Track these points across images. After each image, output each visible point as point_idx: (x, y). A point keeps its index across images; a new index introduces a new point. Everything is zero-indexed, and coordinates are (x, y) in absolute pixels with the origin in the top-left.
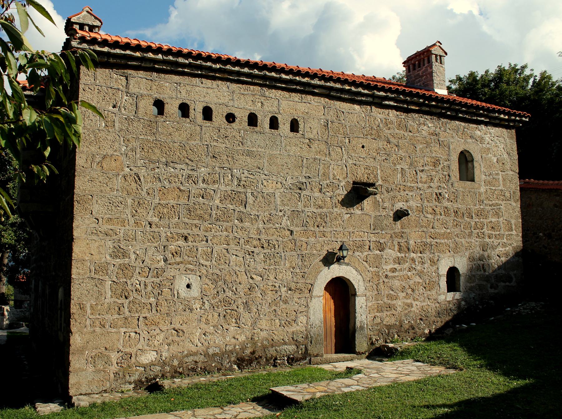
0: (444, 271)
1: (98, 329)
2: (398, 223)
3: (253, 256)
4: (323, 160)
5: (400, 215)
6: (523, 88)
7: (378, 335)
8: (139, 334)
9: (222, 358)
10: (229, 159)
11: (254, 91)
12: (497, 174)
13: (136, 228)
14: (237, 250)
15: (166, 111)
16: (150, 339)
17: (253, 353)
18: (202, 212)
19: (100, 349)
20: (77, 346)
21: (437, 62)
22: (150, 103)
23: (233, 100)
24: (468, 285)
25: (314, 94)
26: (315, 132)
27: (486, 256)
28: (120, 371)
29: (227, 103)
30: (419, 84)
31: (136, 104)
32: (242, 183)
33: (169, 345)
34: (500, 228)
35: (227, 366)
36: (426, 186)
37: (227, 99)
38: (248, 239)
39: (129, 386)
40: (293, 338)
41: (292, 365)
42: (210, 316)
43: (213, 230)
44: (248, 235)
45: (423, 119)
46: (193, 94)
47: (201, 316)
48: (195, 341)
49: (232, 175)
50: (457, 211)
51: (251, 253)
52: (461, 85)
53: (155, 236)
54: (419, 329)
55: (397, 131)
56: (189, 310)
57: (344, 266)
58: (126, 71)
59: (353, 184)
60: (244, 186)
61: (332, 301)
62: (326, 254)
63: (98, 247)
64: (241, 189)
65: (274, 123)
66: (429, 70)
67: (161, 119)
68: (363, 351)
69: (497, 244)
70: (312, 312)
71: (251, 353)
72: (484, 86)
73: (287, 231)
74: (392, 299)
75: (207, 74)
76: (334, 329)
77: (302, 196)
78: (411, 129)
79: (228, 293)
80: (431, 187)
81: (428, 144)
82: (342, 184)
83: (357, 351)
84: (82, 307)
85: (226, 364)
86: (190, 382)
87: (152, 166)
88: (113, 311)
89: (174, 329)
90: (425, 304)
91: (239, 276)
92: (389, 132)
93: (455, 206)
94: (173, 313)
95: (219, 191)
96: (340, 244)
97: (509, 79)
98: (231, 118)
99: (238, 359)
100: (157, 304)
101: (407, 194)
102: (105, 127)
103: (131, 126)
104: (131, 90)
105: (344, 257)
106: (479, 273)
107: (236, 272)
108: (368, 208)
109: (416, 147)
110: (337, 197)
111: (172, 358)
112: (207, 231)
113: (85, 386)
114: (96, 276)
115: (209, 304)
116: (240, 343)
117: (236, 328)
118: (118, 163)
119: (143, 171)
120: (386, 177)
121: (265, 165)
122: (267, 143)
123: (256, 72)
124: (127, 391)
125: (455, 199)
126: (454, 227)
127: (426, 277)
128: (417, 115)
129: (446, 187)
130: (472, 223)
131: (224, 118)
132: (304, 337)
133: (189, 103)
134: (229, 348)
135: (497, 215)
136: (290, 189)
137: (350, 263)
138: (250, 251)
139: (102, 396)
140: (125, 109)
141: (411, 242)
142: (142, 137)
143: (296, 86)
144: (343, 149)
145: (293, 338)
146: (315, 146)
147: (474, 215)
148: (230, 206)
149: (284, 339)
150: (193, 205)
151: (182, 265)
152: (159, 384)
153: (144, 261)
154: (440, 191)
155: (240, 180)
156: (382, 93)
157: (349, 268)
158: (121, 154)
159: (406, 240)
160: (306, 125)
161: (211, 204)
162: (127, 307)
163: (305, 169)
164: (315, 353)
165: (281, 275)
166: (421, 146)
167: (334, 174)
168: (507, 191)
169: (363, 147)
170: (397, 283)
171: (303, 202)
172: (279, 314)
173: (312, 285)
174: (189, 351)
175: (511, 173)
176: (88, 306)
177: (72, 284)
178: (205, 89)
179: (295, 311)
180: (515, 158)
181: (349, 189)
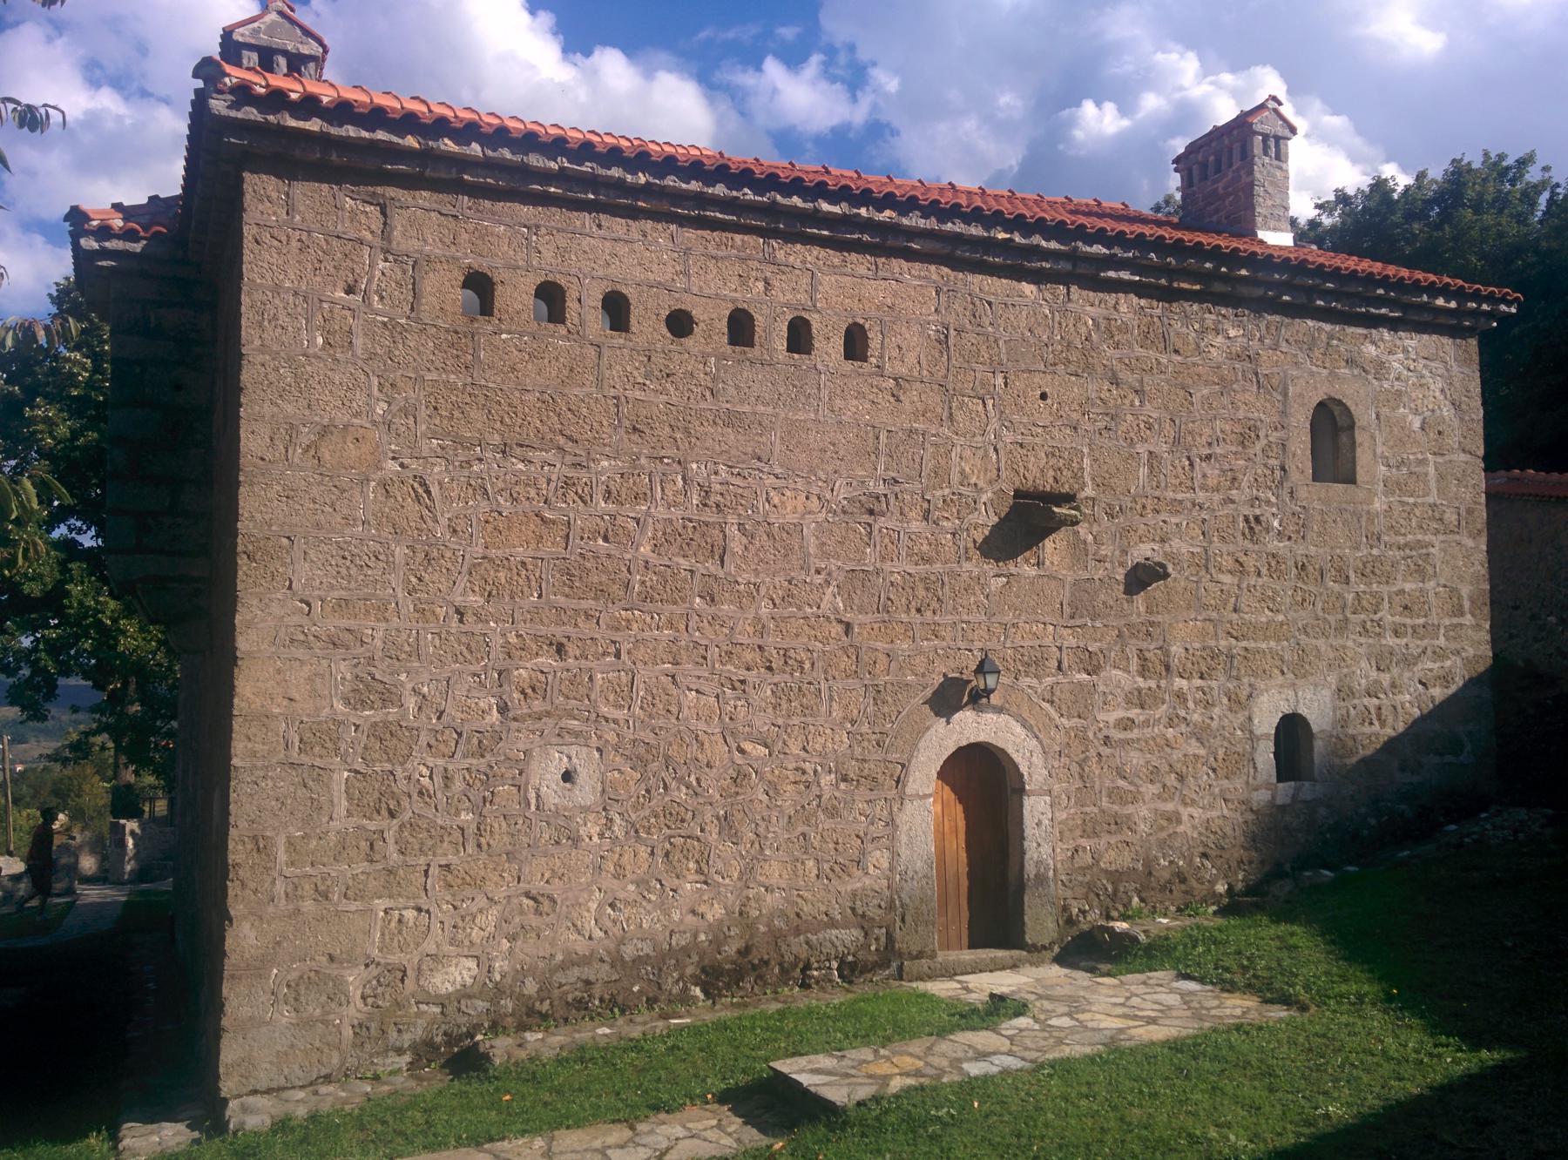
0: (1266, 721)
1: (308, 905)
2: (1140, 600)
3: (744, 691)
5: (1142, 578)
6: (1521, 219)
7: (1086, 898)
8: (428, 912)
9: (660, 970)
10: (678, 436)
11: (744, 247)
12: (1423, 462)
13: (421, 624)
14: (699, 678)
16: (460, 924)
17: (745, 952)
18: (604, 578)
19: (312, 959)
20: (247, 955)
21: (1266, 153)
22: (454, 283)
23: (686, 274)
25: (910, 255)
26: (911, 359)
27: (1386, 684)
28: (371, 1019)
29: (669, 283)
30: (1214, 219)
31: (414, 284)
32: (714, 498)
33: (512, 938)
34: (1426, 607)
35: (674, 991)
36: (1217, 497)
37: (670, 269)
38: (730, 648)
39: (397, 1059)
40: (853, 909)
41: (851, 982)
42: (626, 857)
43: (635, 626)
44: (729, 637)
45: (1213, 317)
46: (574, 258)
47: (602, 857)
48: (586, 925)
49: (684, 479)
50: (1303, 565)
51: (738, 685)
52: (1348, 215)
53: (473, 645)
54: (1200, 880)
55: (1139, 351)
56: (570, 842)
57: (990, 715)
58: (379, 190)
59: (1015, 497)
60: (718, 506)
61: (960, 808)
62: (941, 684)
63: (310, 680)
64: (710, 516)
65: (800, 337)
66: (1245, 179)
67: (485, 326)
68: (1046, 942)
69: (1419, 650)
70: (904, 839)
71: (739, 952)
72: (1410, 216)
73: (834, 624)
74: (1124, 802)
75: (611, 201)
76: (965, 883)
77: (875, 532)
78: (1179, 345)
79: (676, 793)
80: (1233, 502)
81: (1225, 386)
82: (984, 498)
83: (1030, 942)
84: (261, 846)
85: (671, 985)
86: (569, 1039)
87: (462, 455)
88: (353, 853)
89: (528, 895)
90: (1215, 814)
91: (707, 745)
92: (1117, 353)
93: (1300, 550)
94: (525, 852)
95: (651, 520)
96: (979, 655)
97: (1481, 195)
98: (680, 324)
99: (703, 970)
100: (479, 829)
101: (1164, 522)
102: (323, 349)
103: (401, 347)
104: (398, 244)
105: (988, 692)
107: (697, 736)
108: (1056, 559)
110: (973, 531)
111: (521, 974)
112: (617, 629)
113: (268, 1066)
114: (305, 759)
116: (710, 925)
117: (699, 885)
118: (366, 448)
119: (437, 469)
120: (1107, 476)
121: (777, 450)
122: (782, 390)
123: (748, 194)
124: (391, 1073)
125: (1298, 532)
126: (1296, 607)
127: (1218, 741)
128: (1195, 307)
129: (1273, 499)
131: (663, 325)
132: (883, 904)
133: (563, 282)
134: (679, 941)
135: (1420, 573)
136: (844, 512)
138: (734, 678)
139: (316, 1093)
140: (382, 298)
141: (1173, 649)
142: (433, 376)
143: (862, 233)
144: (990, 403)
145: (853, 909)
146: (911, 397)
147: (1352, 576)
148: (681, 561)
149: (831, 911)
150: (579, 559)
151: (550, 722)
152: (482, 1050)
153: (442, 713)
154: (1258, 512)
155: (706, 492)
156: (1098, 249)
157: (1004, 718)
158: (374, 423)
159: (1161, 643)
160: (887, 340)
161: (628, 556)
162: (393, 841)
163: (883, 459)
164: (915, 950)
165: (821, 740)
166: (1205, 391)
167: (962, 472)
168: (1448, 507)
169: (1044, 396)
170: (1135, 759)
171: (878, 548)
172: (816, 844)
173: (903, 766)
174: (567, 952)
175: (1463, 457)
176: (281, 841)
177: (232, 783)
178: (607, 244)
180: (1474, 416)
181: (1004, 511)
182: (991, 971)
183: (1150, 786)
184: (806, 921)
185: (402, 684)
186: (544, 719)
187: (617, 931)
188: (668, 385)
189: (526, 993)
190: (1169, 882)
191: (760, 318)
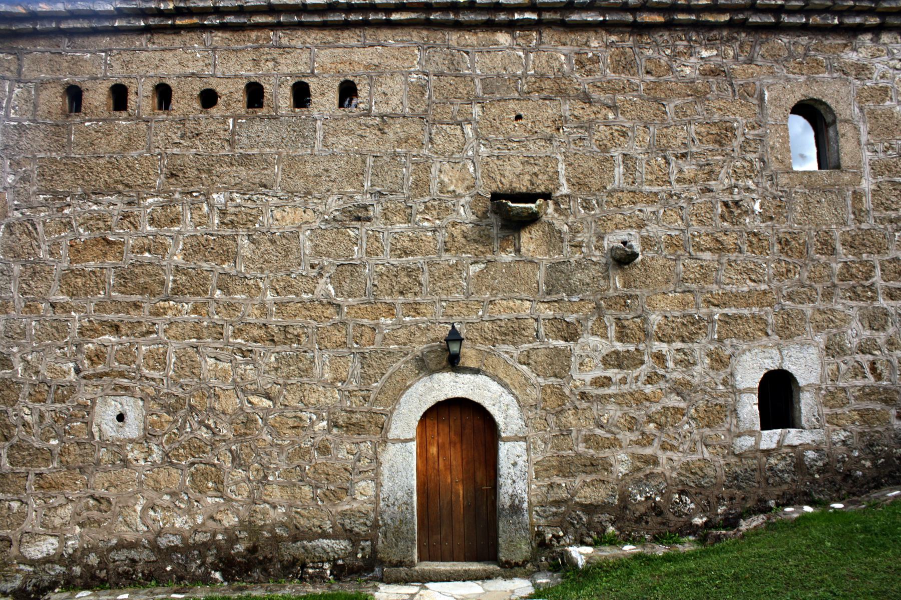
4: (414, 156)
14: (216, 348)
15: (85, 103)
17: (252, 550)
24: (826, 411)
26: (395, 101)
36: (694, 189)
46: (135, 67)
68: (520, 560)
71: (248, 549)
80: (711, 191)
83: (504, 559)
89: (92, 497)
93: (783, 228)
104: (25, 76)
106: (860, 382)
108: (532, 247)
109: (664, 105)
111: (85, 552)
112: (158, 315)
115: (160, 452)
116: (226, 529)
117: (217, 500)
127: (699, 396)
130: (834, 265)
134: (200, 538)
137: (484, 368)
142: (42, 155)
154: (737, 198)
157: (481, 379)
164: (395, 559)
165: (316, 395)
167: (442, 183)
178: (157, 53)
179: (346, 469)
182: (464, 581)
183: (627, 433)
184: (303, 532)
185: (14, 354)
186: (105, 378)
187: (156, 527)
188: (197, 142)
189: (90, 563)
190: (645, 514)
191: (268, 87)
